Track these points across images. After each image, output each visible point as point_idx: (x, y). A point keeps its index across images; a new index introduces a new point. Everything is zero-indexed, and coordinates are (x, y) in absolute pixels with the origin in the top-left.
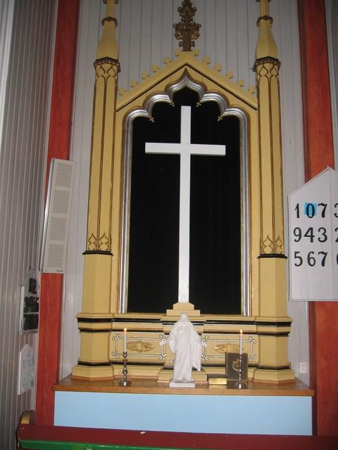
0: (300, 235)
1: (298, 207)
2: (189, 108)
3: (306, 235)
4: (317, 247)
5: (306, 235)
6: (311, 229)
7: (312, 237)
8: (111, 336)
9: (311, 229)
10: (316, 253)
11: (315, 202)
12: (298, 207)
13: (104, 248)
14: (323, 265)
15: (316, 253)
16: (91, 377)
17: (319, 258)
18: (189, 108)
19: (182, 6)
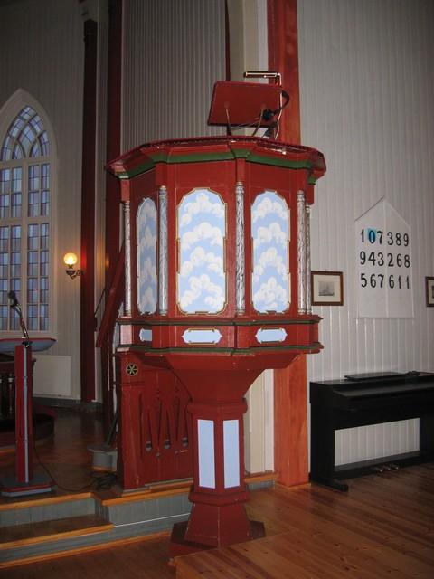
0: (364, 259)
1: (363, 232)
2: (202, 483)
3: (370, 259)
4: (377, 270)
5: (370, 259)
6: (373, 253)
7: (374, 260)
8: (211, 256)
9: (373, 253)
10: (377, 275)
11: (376, 229)
12: (363, 232)
13: (31, 227)
14: (381, 286)
15: (377, 275)
16: (17, 524)
17: (378, 280)
18: (202, 483)
19: (189, 248)
